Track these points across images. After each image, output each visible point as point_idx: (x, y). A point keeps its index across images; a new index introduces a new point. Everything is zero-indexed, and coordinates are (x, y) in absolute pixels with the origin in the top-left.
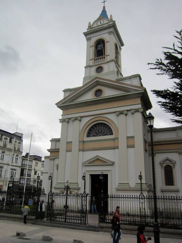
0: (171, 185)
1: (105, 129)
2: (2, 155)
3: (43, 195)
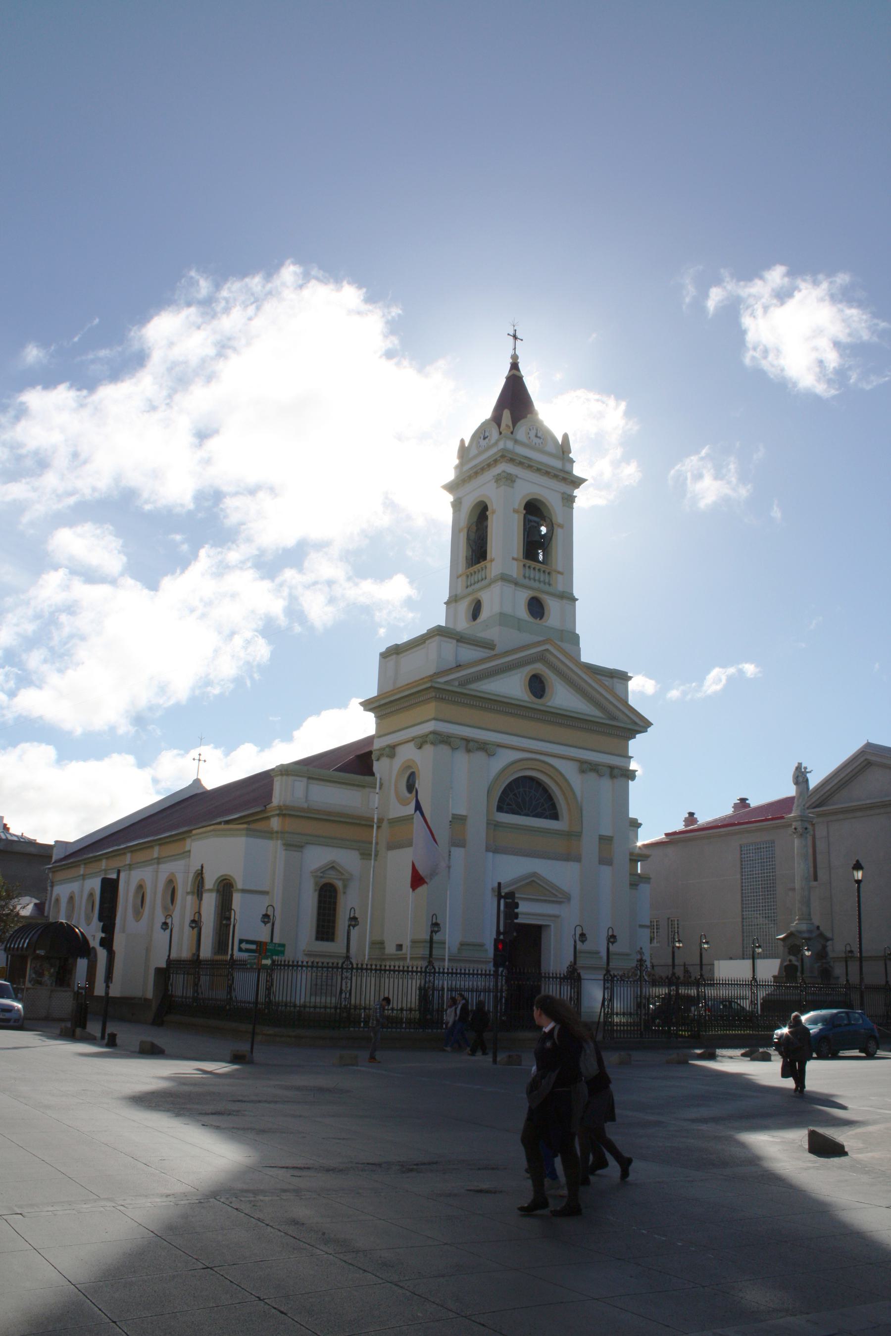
0: (327, 940)
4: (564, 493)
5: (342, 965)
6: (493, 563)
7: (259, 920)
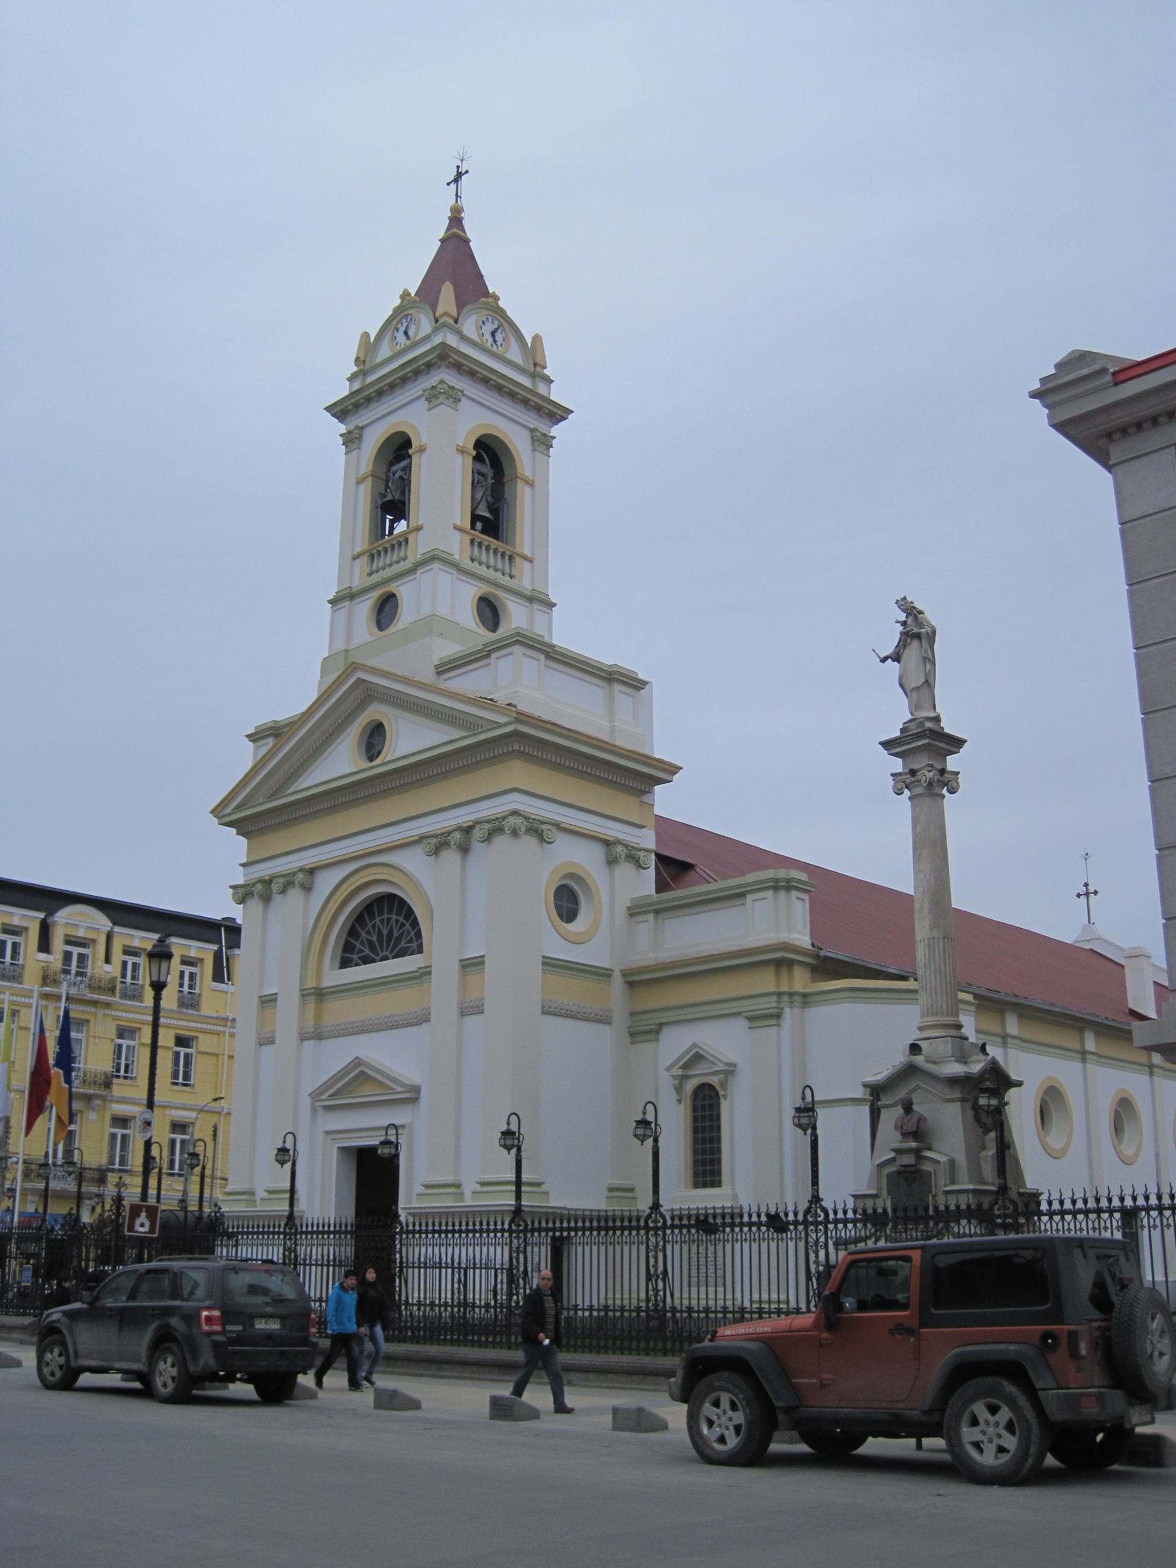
1: (389, 919)
2: (177, 1054)
3: (595, 1233)
4: (532, 431)
6: (421, 533)
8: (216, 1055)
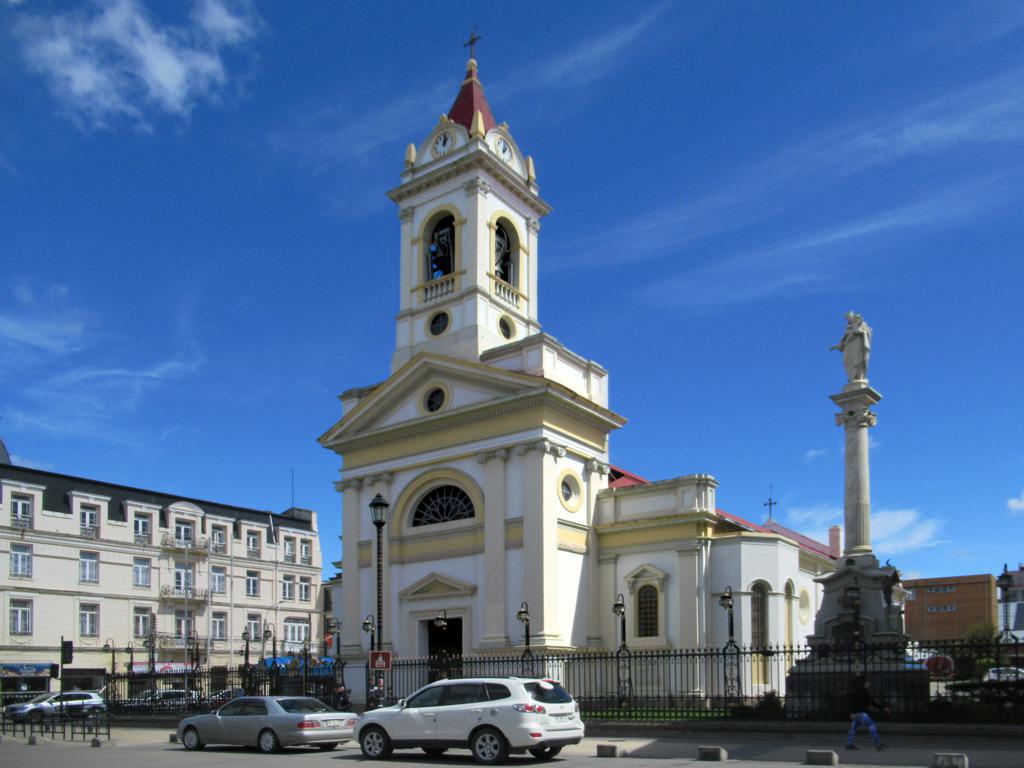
0: (651, 635)
1: (447, 500)
5: (724, 650)
6: (464, 276)
7: (611, 610)
8: (272, 581)
